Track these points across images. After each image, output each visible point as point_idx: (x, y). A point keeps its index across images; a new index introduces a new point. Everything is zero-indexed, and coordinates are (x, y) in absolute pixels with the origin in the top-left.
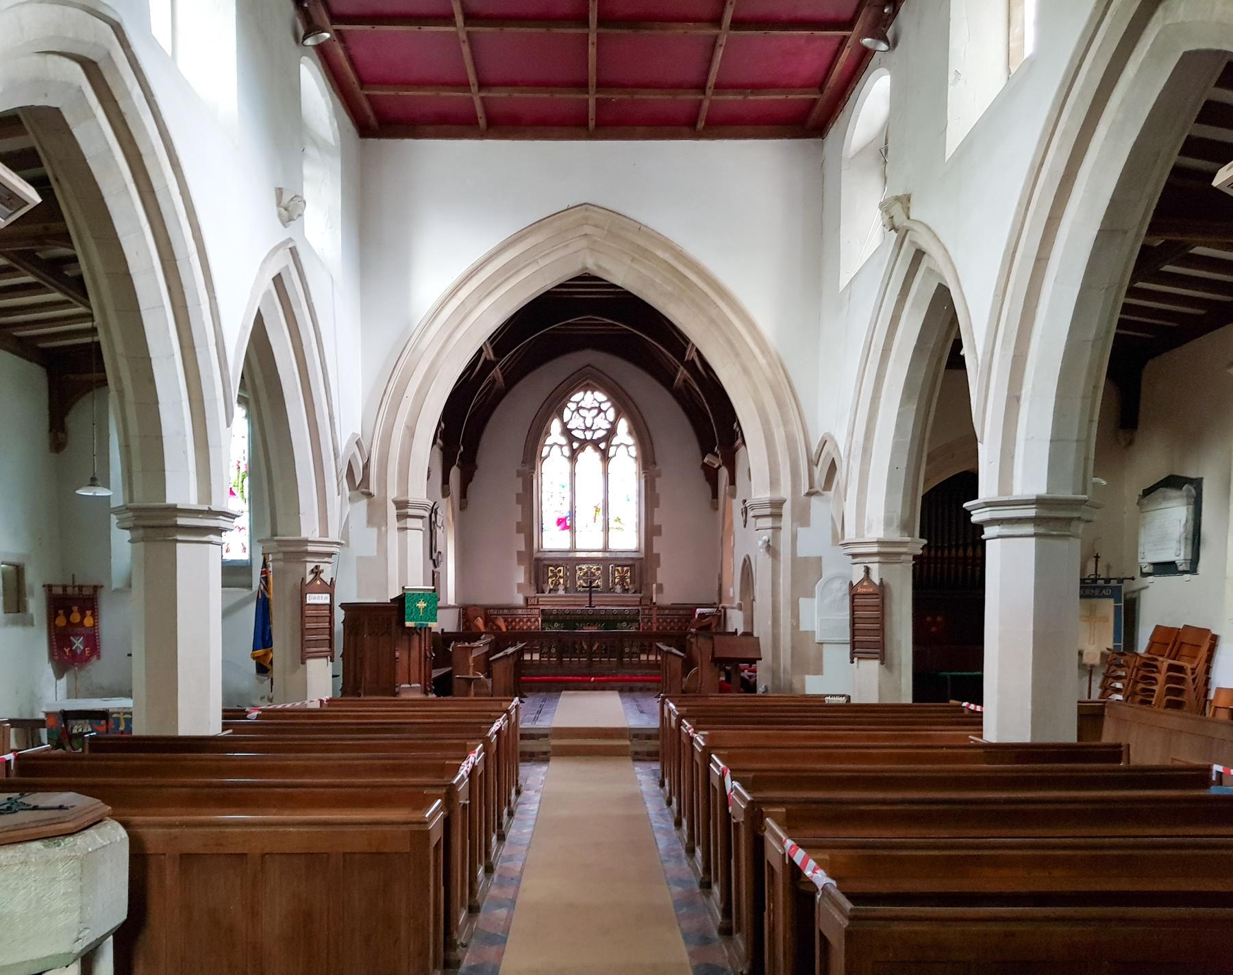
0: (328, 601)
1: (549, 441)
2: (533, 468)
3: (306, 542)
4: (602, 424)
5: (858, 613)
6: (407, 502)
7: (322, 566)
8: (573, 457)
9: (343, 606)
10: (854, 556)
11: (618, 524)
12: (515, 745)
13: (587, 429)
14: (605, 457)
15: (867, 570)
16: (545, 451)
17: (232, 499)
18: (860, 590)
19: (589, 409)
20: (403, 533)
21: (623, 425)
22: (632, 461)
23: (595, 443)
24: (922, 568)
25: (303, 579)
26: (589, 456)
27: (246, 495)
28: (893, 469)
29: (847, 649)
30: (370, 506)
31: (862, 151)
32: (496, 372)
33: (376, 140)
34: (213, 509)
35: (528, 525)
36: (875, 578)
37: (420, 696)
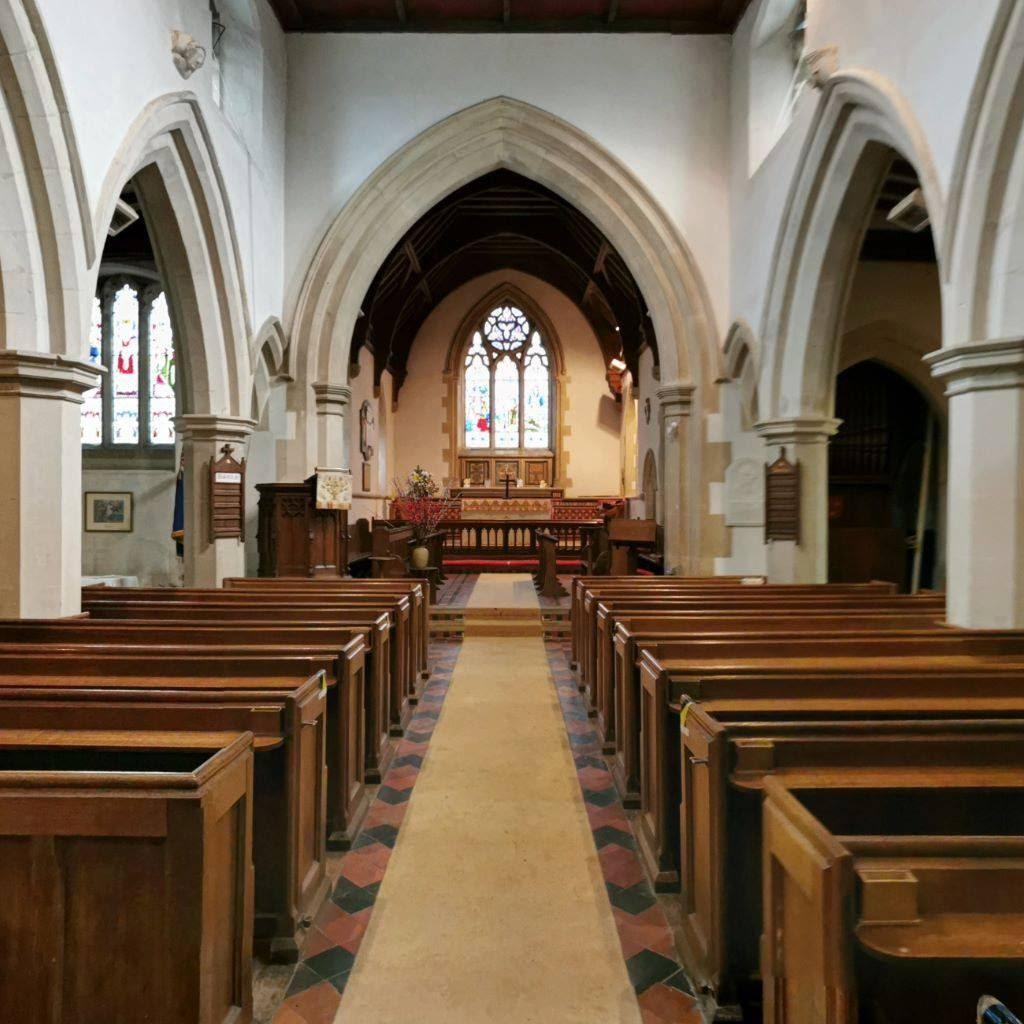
0: (238, 481)
1: (472, 351)
2: (457, 375)
3: (214, 420)
4: (519, 335)
5: (775, 494)
6: (326, 387)
7: (232, 445)
8: (492, 367)
9: (259, 487)
10: (769, 436)
11: (532, 426)
12: (423, 626)
13: (505, 341)
14: (521, 366)
15: (783, 451)
16: (468, 360)
17: (159, 386)
18: (776, 471)
19: (506, 323)
20: (322, 418)
21: (536, 338)
22: (545, 369)
23: (512, 354)
24: (838, 450)
25: (212, 458)
26: (507, 367)
27: (173, 381)
28: (810, 346)
29: (760, 532)
30: (290, 389)
31: (771, 38)
32: (423, 285)
33: (299, 34)
34: (64, 358)
35: (452, 426)
36: (791, 458)
37: (334, 577)
